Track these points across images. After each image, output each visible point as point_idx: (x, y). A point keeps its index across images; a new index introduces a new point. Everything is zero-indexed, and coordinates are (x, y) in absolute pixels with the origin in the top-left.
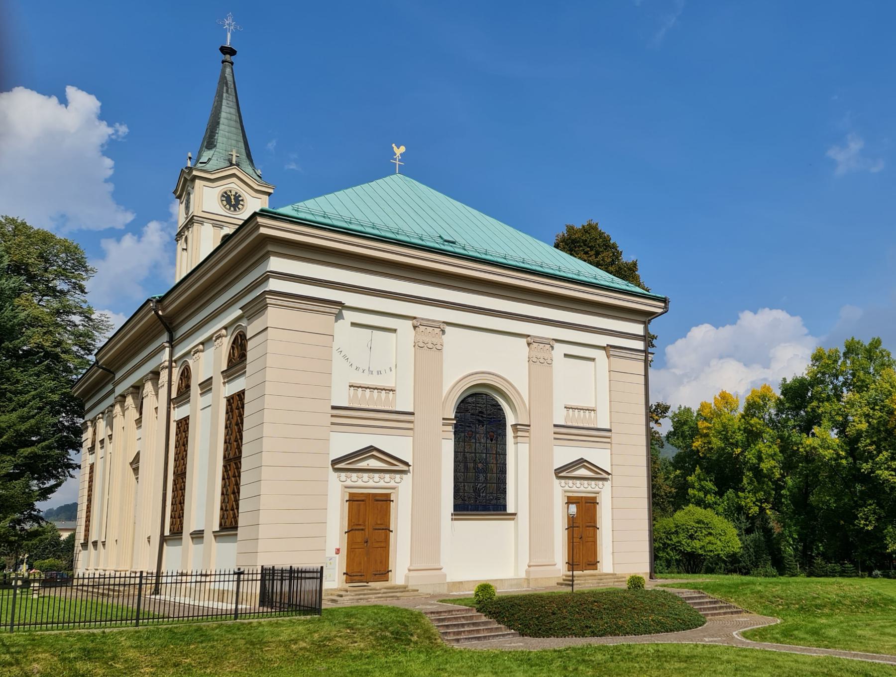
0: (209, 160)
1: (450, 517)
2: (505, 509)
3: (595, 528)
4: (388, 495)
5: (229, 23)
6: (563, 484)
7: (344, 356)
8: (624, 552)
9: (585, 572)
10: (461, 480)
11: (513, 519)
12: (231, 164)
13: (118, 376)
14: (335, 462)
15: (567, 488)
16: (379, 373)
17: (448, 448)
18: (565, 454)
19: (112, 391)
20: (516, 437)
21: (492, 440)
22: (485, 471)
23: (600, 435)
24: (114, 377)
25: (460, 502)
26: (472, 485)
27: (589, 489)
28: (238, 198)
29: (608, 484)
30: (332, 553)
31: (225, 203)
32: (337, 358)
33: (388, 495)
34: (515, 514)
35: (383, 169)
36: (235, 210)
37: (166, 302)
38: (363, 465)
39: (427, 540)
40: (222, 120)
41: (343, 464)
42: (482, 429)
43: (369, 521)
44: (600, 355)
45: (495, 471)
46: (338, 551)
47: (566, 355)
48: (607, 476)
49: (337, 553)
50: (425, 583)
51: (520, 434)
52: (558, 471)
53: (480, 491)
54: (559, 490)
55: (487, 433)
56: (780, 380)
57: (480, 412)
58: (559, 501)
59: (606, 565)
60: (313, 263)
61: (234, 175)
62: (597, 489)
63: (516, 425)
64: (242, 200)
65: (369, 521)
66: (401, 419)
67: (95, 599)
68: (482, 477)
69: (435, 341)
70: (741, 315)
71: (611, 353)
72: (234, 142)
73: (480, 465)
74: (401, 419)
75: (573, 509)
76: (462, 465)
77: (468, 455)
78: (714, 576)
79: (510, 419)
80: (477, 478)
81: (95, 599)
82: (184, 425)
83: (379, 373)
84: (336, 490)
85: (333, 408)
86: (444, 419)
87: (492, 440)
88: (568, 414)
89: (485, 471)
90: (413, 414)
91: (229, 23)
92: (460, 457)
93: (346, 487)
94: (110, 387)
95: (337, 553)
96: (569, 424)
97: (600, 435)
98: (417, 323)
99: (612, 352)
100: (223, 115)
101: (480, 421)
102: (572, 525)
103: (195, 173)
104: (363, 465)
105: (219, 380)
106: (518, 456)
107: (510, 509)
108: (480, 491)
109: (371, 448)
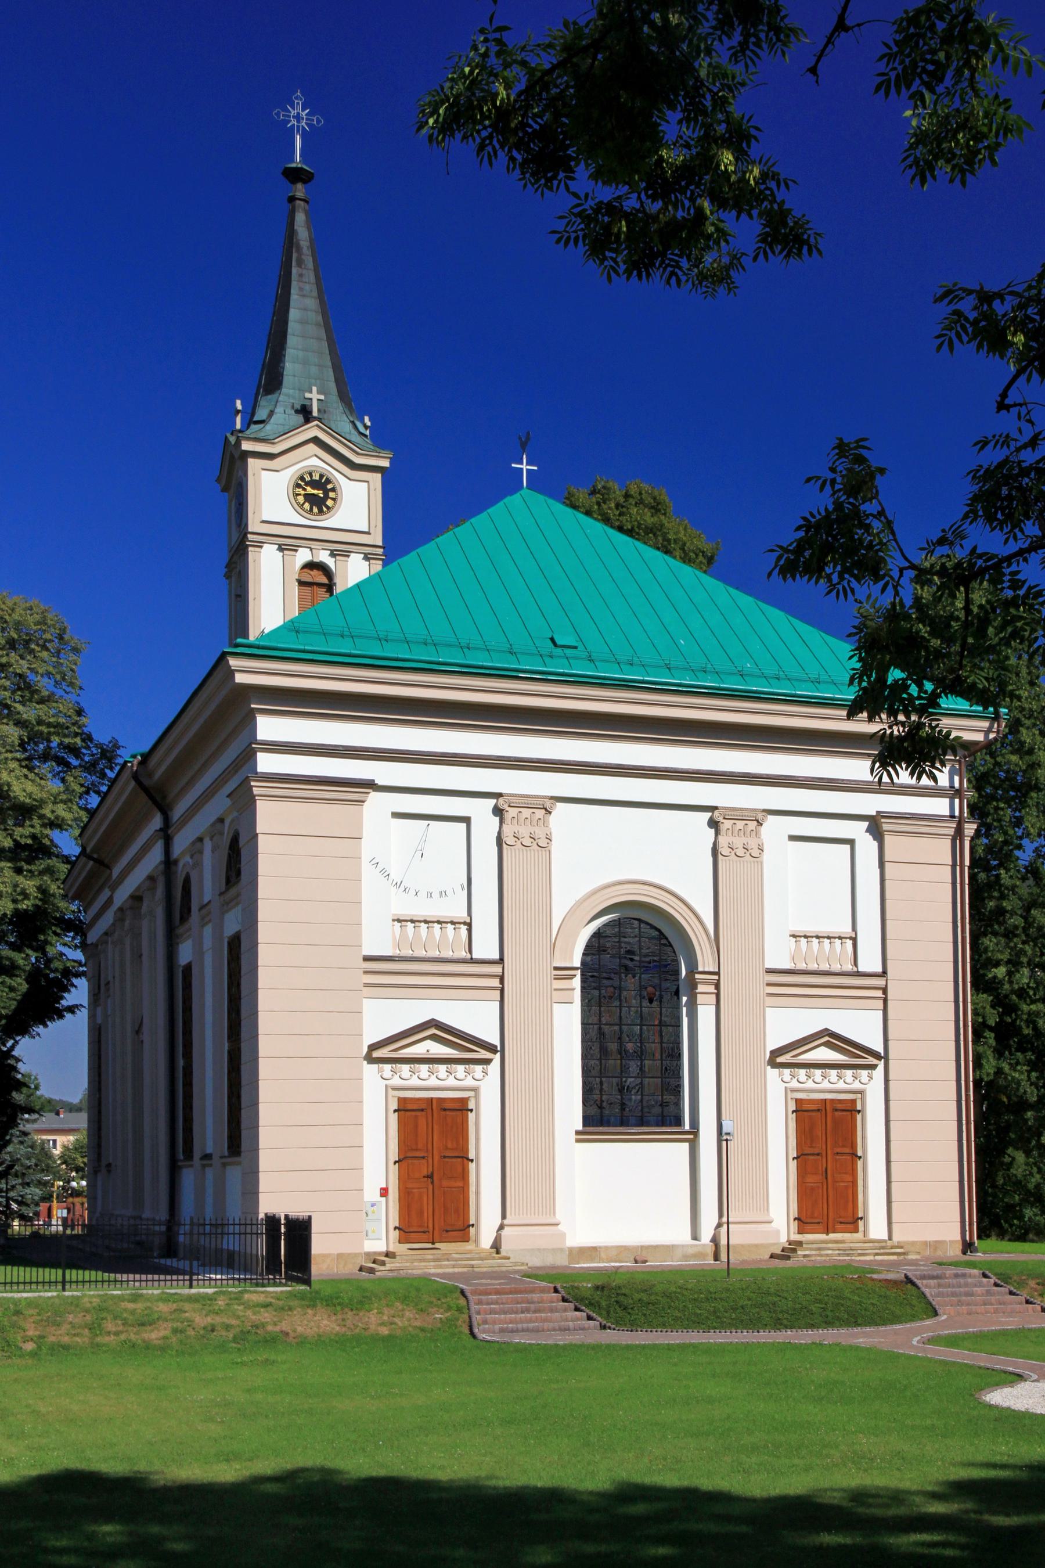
0: (271, 413)
1: (574, 1137)
5: (298, 115)
6: (787, 1078)
9: (832, 1236)
10: (594, 1073)
13: (116, 871)
16: (443, 894)
19: (109, 902)
21: (651, 1001)
22: (641, 1054)
24: (111, 874)
25: (594, 1111)
26: (615, 1080)
27: (841, 1085)
28: (323, 484)
30: (376, 1196)
32: (369, 875)
33: (464, 1101)
35: (512, 484)
36: (321, 512)
37: (153, 762)
39: (530, 1180)
41: (382, 1052)
42: (631, 983)
43: (433, 1144)
45: (658, 1056)
46: (384, 1192)
49: (382, 1195)
50: (526, 1248)
53: (635, 1081)
55: (642, 988)
57: (629, 952)
61: (316, 440)
64: (333, 490)
65: (433, 1144)
68: (633, 1067)
70: (932, 799)
72: (314, 370)
73: (630, 1046)
76: (596, 1049)
77: (606, 1028)
78: (1026, 1246)
80: (624, 1070)
83: (443, 894)
84: (376, 1093)
85: (367, 959)
86: (556, 969)
87: (651, 1001)
88: (798, 947)
89: (641, 1054)
91: (298, 115)
92: (593, 1033)
94: (106, 893)
95: (382, 1195)
100: (294, 314)
103: (246, 446)
108: (635, 1081)
109: (826, 1032)
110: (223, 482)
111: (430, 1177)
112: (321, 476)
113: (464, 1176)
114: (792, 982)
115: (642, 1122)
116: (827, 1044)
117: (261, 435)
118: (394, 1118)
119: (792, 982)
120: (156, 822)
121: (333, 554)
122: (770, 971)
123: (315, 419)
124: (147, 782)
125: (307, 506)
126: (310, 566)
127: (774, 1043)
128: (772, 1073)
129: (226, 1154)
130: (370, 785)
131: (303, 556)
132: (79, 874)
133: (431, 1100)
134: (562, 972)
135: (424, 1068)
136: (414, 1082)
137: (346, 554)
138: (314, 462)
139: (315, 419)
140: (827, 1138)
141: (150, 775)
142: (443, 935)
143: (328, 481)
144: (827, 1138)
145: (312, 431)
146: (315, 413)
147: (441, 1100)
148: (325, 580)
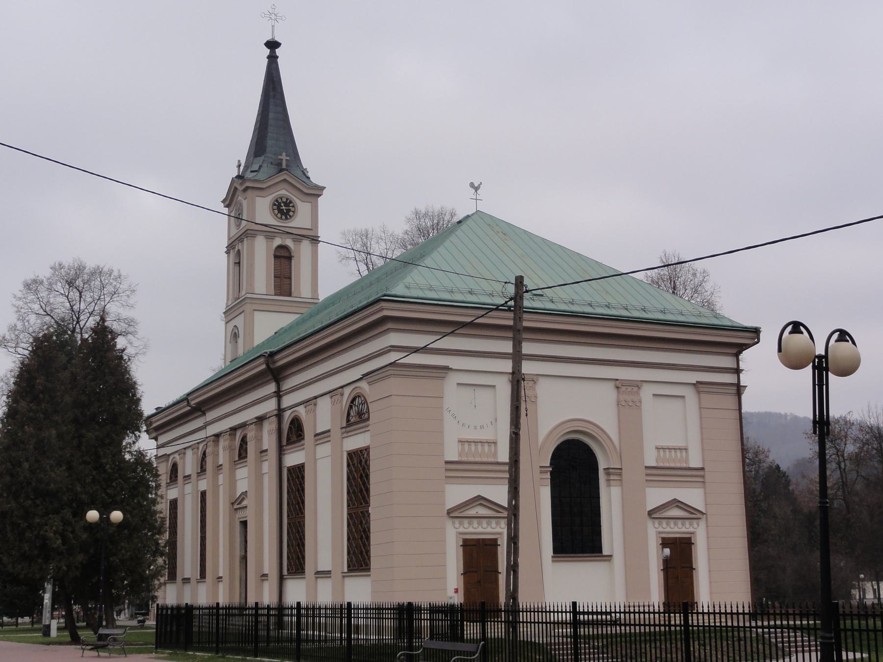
2: (601, 552)
3: (691, 569)
4: (690, 539)
7: (453, 415)
11: (609, 561)
12: (281, 170)
14: (449, 512)
15: (661, 529)
16: (482, 427)
18: (657, 496)
20: (608, 480)
23: (694, 475)
28: (288, 203)
29: (702, 523)
31: (276, 211)
32: (447, 417)
34: (611, 556)
36: (286, 218)
37: (277, 357)
38: (472, 512)
40: (271, 122)
46: (456, 591)
47: (654, 395)
48: (699, 515)
51: (612, 477)
52: (650, 513)
53: (577, 533)
54: (653, 533)
58: (653, 544)
62: (691, 530)
63: (608, 469)
67: (736, 633)
71: (701, 389)
75: (667, 551)
81: (736, 633)
82: (297, 475)
83: (482, 427)
86: (541, 467)
96: (661, 465)
97: (694, 475)
99: (702, 388)
102: (668, 566)
104: (472, 512)
105: (336, 433)
106: (611, 501)
107: (606, 551)
108: (577, 533)
109: (479, 498)
110: (227, 202)
111: (480, 582)
112: (287, 199)
113: (691, 577)
114: (660, 474)
115: (583, 552)
116: (677, 506)
117: (257, 178)
118: (461, 549)
119: (660, 474)
120: (271, 388)
121: (294, 240)
122: (647, 467)
123: (284, 170)
124: (272, 366)
125: (279, 215)
126: (281, 247)
127: (450, 505)
128: (650, 523)
129: (346, 570)
130: (447, 368)
131: (278, 242)
132: (173, 413)
133: (479, 540)
134: (614, 473)
135: (475, 522)
136: (471, 530)
137: (300, 241)
138: (283, 192)
139: (284, 170)
140: (679, 559)
141: (274, 362)
142: (676, 455)
143: (291, 202)
144: (679, 559)
145: (283, 176)
146: (284, 166)
147: (484, 540)
148: (287, 254)
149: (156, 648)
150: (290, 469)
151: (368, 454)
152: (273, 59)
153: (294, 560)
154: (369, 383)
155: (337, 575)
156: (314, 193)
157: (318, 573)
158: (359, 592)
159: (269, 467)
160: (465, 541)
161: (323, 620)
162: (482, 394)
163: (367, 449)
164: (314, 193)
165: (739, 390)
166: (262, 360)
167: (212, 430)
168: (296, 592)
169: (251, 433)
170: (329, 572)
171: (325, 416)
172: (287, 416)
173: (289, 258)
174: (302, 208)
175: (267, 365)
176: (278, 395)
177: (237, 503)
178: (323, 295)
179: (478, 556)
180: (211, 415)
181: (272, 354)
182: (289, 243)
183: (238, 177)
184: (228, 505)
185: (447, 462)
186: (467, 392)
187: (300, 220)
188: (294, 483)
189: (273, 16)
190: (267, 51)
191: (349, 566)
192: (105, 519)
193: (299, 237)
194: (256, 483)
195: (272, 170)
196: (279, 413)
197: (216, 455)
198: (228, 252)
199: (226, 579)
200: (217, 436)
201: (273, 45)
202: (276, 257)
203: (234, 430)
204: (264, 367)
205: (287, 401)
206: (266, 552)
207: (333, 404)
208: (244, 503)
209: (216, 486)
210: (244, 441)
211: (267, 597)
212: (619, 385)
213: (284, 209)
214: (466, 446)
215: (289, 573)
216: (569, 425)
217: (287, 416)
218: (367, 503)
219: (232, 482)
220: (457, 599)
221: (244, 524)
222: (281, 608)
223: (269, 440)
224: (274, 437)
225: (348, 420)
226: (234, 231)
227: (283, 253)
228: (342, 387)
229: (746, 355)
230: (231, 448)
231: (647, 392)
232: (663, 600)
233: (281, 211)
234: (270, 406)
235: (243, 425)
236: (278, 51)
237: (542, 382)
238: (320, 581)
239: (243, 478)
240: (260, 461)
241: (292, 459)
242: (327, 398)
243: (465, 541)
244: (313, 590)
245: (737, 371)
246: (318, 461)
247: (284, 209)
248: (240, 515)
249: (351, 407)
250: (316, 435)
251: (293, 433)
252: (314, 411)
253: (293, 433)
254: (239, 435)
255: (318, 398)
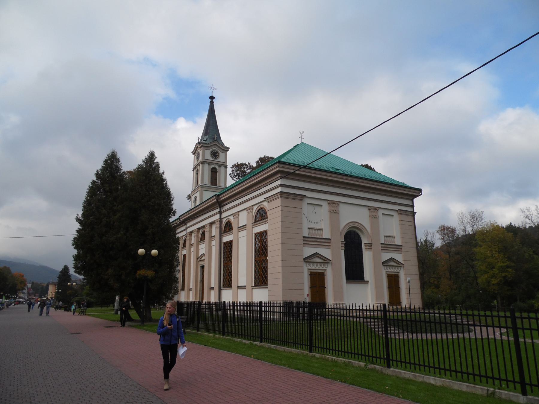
2: (364, 279)
4: (324, 273)
8: (410, 297)
14: (304, 259)
16: (317, 223)
17: (343, 252)
18: (386, 256)
23: (398, 248)
30: (306, 296)
32: (304, 217)
33: (324, 273)
38: (314, 260)
39: (339, 293)
41: (307, 260)
44: (325, 204)
46: (308, 295)
48: (401, 265)
53: (355, 273)
56: (91, 168)
59: (405, 303)
60: (404, 216)
66: (326, 242)
69: (336, 209)
74: (326, 242)
79: (364, 241)
82: (229, 246)
83: (317, 223)
90: (330, 239)
93: (309, 269)
98: (330, 202)
101: (353, 243)
104: (314, 260)
105: (249, 226)
106: (367, 257)
107: (367, 277)
119: (387, 247)
126: (214, 168)
131: (212, 166)
136: (313, 268)
140: (393, 281)
144: (393, 281)
149: (143, 323)
150: (225, 243)
151: (267, 234)
152: (212, 103)
153: (227, 280)
154: (268, 202)
155: (249, 287)
156: (226, 149)
157: (238, 287)
158: (261, 296)
159: (215, 243)
160: (311, 272)
161: (214, 313)
162: (317, 208)
163: (266, 231)
164: (226, 149)
165: (414, 213)
166: (215, 197)
167: (189, 230)
168: (228, 296)
169: (207, 230)
170: (245, 286)
171: (244, 219)
172: (224, 221)
173: (216, 172)
174: (222, 155)
175: (217, 199)
176: (220, 213)
177: (199, 259)
178: (228, 185)
179: (318, 281)
180: (188, 225)
181: (219, 195)
182: (217, 167)
183: (198, 143)
184: (195, 259)
185: (304, 237)
186: (311, 207)
187: (221, 159)
188: (227, 250)
189: (212, 88)
190: (210, 100)
191: (255, 284)
192: (148, 251)
193: (220, 165)
194: (210, 251)
195: (211, 141)
196: (221, 219)
197: (190, 240)
198: (193, 170)
199: (194, 290)
200: (191, 232)
201: (212, 98)
202: (212, 171)
203: (199, 229)
204: (215, 200)
205: (224, 215)
206: (213, 277)
207: (248, 213)
208: (203, 258)
209: (190, 252)
210: (204, 233)
211: (213, 298)
212: (370, 208)
213: (215, 155)
214: (311, 231)
215: (224, 287)
216: (348, 226)
217: (224, 221)
218: (266, 255)
219: (198, 250)
220: (308, 300)
221: (203, 267)
222: (220, 303)
223: (215, 231)
224: (218, 230)
225: (255, 220)
226: (196, 163)
227: (214, 170)
228: (252, 206)
229: (415, 200)
230: (197, 237)
231: (381, 212)
232: (389, 301)
233: (214, 155)
234: (217, 217)
235: (203, 227)
236: (214, 100)
237: (341, 205)
238: (239, 291)
239: (203, 249)
240: (210, 241)
241: (226, 239)
242: (245, 211)
243: (311, 272)
244: (236, 295)
245: (413, 206)
246: (239, 239)
247: (215, 155)
248: (201, 263)
249: (257, 214)
250: (239, 228)
251: (228, 227)
252: (238, 218)
253: (228, 227)
254: (201, 231)
255: (240, 213)
